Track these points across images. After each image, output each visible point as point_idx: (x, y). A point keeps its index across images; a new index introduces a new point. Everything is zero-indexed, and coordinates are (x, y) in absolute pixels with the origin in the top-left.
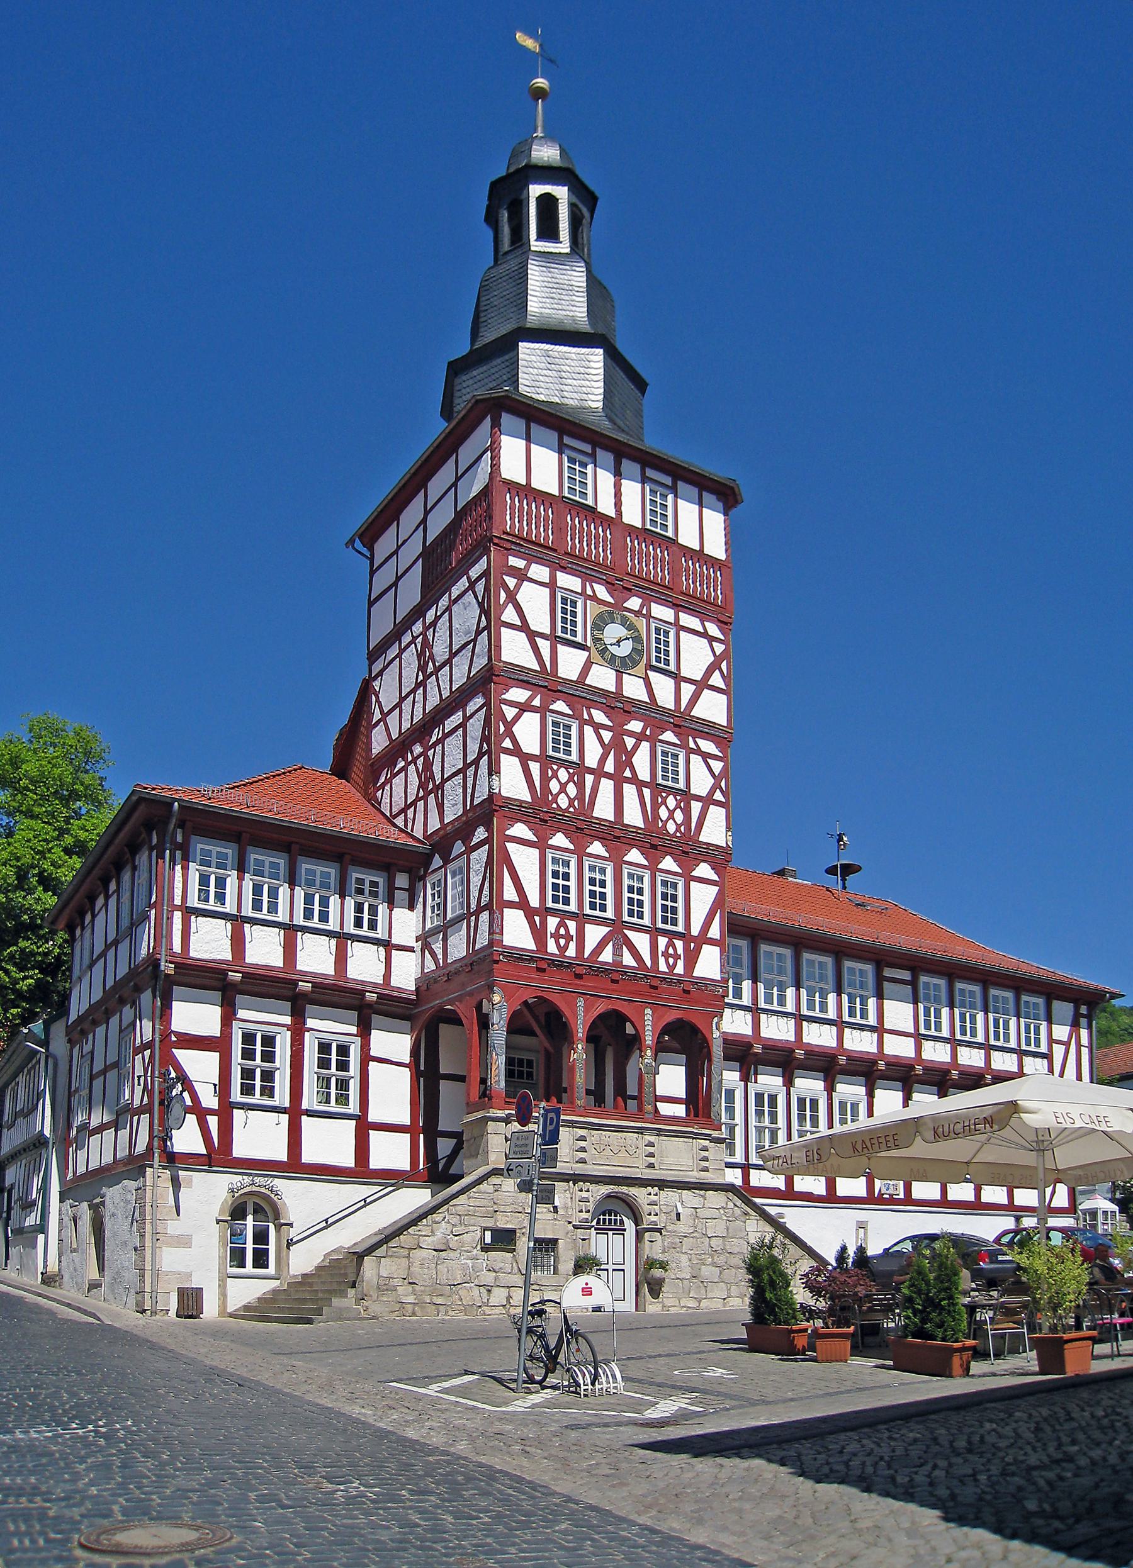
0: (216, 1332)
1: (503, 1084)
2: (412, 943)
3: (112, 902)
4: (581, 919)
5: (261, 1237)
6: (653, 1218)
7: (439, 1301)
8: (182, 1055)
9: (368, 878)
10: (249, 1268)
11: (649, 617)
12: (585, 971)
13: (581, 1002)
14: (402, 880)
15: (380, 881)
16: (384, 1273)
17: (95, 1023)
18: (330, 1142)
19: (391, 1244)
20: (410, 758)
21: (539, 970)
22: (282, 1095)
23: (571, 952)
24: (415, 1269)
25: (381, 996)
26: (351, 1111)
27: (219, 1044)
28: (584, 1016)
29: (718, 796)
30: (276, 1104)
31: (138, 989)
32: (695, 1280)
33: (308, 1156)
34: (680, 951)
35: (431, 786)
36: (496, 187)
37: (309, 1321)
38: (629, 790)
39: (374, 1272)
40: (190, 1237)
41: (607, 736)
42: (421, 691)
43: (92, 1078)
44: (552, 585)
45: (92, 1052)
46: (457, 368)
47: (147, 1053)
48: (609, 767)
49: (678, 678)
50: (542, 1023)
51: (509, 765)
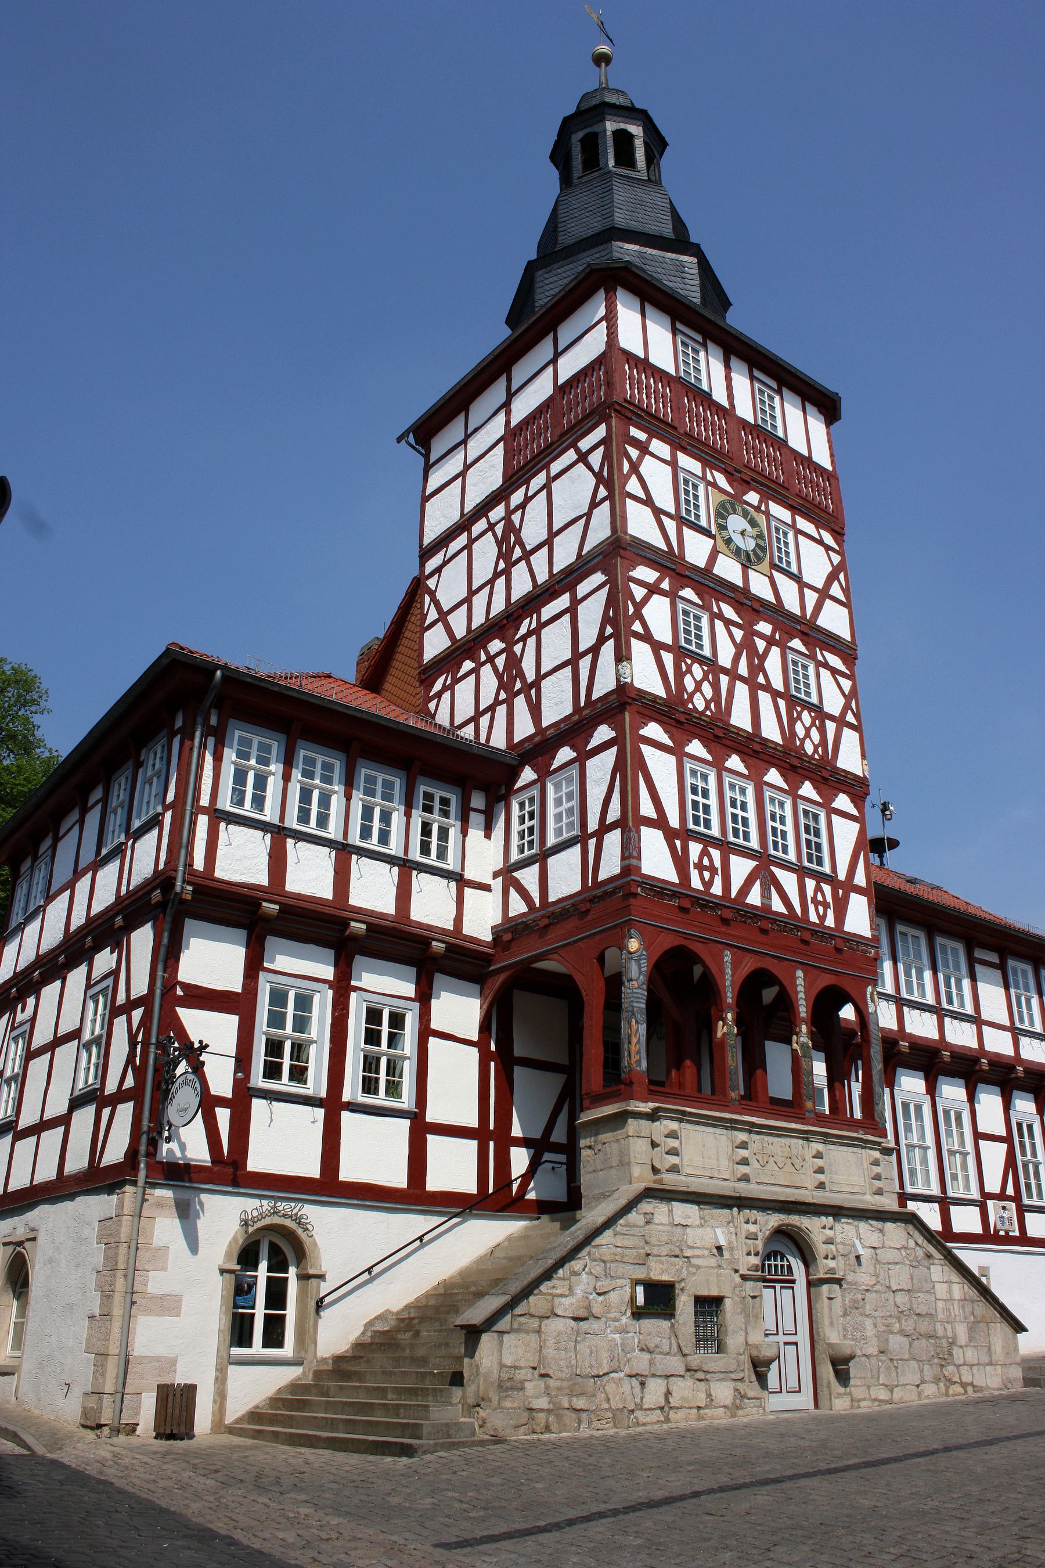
0: (207, 1463)
1: (644, 1064)
2: (488, 879)
3: (93, 819)
4: (727, 848)
5: (276, 1296)
6: (831, 1264)
7: (580, 1403)
8: (188, 1016)
9: (438, 794)
10: (257, 1348)
11: (767, 514)
12: (731, 913)
13: (728, 957)
14: (478, 801)
15: (454, 799)
16: (508, 1360)
18: (375, 1150)
19: (518, 1310)
20: (483, 658)
21: (683, 909)
22: (317, 1083)
23: (717, 889)
24: (549, 1352)
25: (451, 948)
26: (405, 1106)
27: (237, 1004)
28: (732, 976)
29: (850, 718)
30: (310, 1092)
32: (883, 1358)
33: (347, 1173)
34: (829, 899)
35: (518, 685)
36: (568, 125)
37: (407, 1451)
38: (764, 698)
39: (495, 1359)
40: (179, 1298)
41: (738, 634)
42: (502, 581)
44: (673, 463)
45: (33, 1020)
47: (137, 1014)
48: (743, 669)
49: (802, 585)
50: (681, 982)
51: (640, 650)
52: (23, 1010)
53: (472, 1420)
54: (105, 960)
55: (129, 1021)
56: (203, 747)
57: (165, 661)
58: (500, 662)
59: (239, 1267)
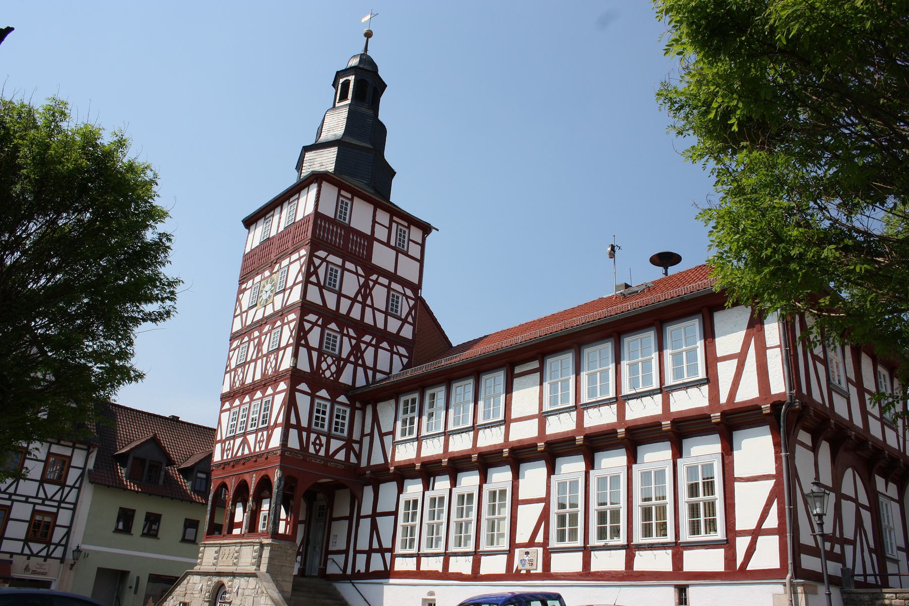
4: (329, 437)
38: (360, 370)
46: (306, 149)
49: (340, 295)
51: (303, 351)
55: (803, 444)
58: (256, 341)
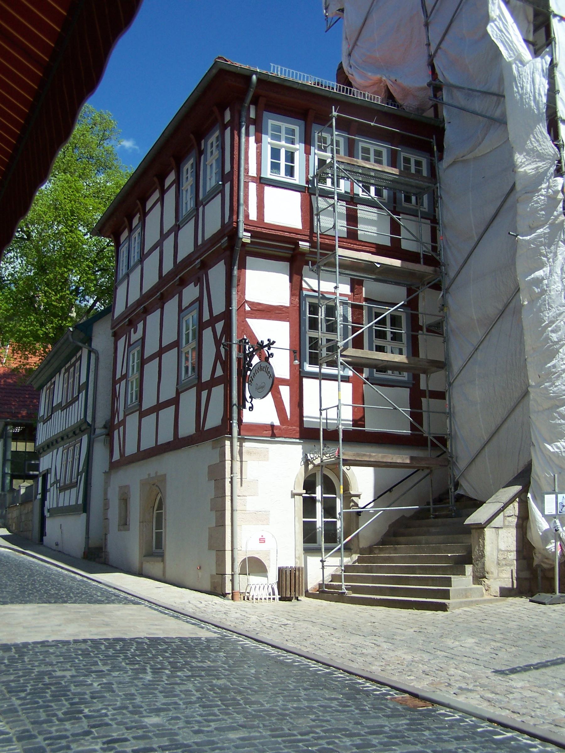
3: (170, 196)
17: (147, 311)
31: (205, 266)
37: (443, 608)
43: (143, 362)
45: (143, 339)
47: (219, 326)
52: (135, 332)
53: (481, 586)
54: (191, 292)
56: (247, 135)
57: (214, 71)
59: (305, 491)
